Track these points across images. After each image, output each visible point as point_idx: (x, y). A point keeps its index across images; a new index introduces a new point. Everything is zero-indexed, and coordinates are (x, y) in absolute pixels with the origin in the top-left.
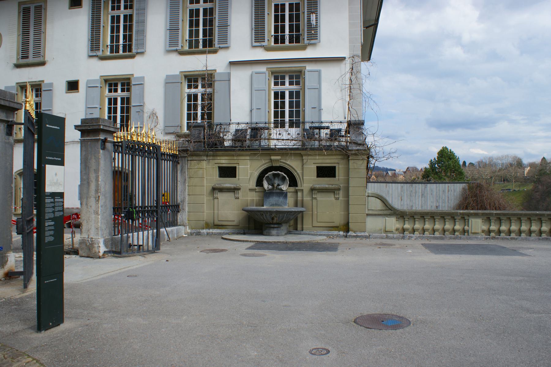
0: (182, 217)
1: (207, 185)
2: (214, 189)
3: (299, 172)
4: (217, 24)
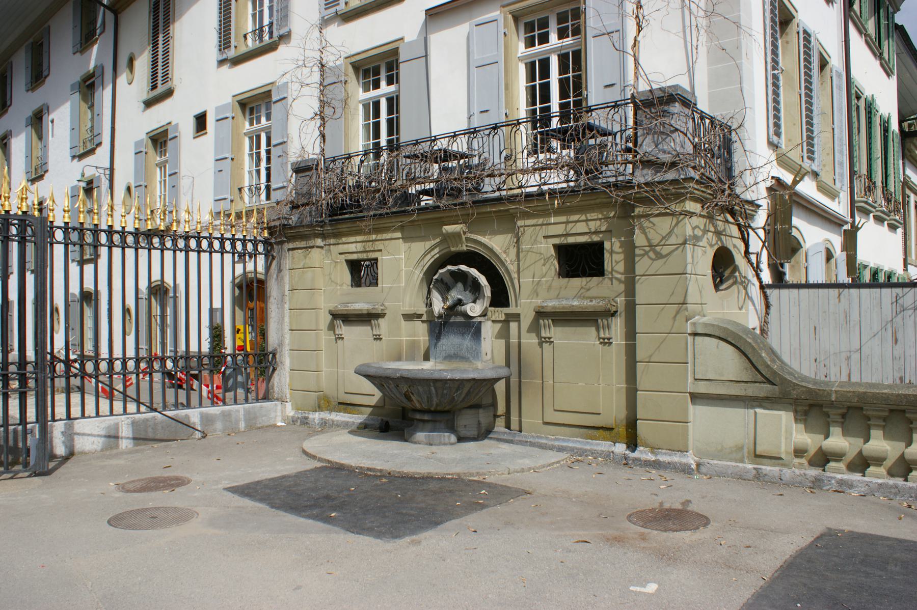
0: (282, 379)
1: (325, 303)
2: (335, 316)
3: (512, 268)
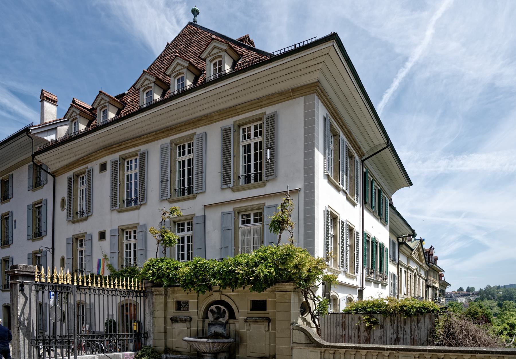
4: (194, 172)
